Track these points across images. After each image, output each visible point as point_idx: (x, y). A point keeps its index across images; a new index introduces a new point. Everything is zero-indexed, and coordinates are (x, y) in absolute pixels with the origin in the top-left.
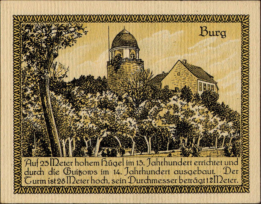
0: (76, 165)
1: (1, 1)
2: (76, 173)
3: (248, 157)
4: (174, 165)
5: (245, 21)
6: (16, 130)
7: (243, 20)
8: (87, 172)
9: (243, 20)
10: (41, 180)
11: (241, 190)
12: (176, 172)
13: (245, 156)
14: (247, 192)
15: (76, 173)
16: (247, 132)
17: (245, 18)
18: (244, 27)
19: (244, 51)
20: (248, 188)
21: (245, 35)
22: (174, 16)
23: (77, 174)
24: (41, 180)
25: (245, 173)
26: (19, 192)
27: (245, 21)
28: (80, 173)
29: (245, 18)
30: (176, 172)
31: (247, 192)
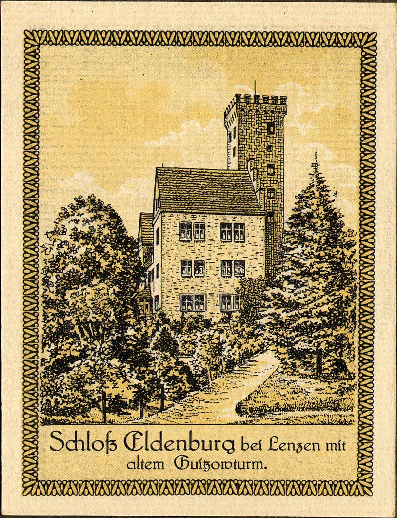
0: (328, 450)
1: (5, 512)
2: (199, 467)
3: (305, 35)
4: (332, 450)
5: (367, 45)
6: (73, 492)
7: (365, 44)
8: (221, 464)
9: (365, 44)
10: (253, 463)
11: (29, 158)
12: (131, 466)
13: (94, 39)
14: (367, 494)
15: (199, 467)
16: (349, 492)
17: (368, 488)
18: (367, 56)
19: (32, 231)
20: (367, 35)
21: (63, 38)
22: (121, 493)
23: (201, 468)
24: (253, 463)
25: (365, 456)
26: (33, 492)
27: (367, 45)
28: (207, 467)
29: (368, 488)
30: (131, 466)
31: (367, 494)
